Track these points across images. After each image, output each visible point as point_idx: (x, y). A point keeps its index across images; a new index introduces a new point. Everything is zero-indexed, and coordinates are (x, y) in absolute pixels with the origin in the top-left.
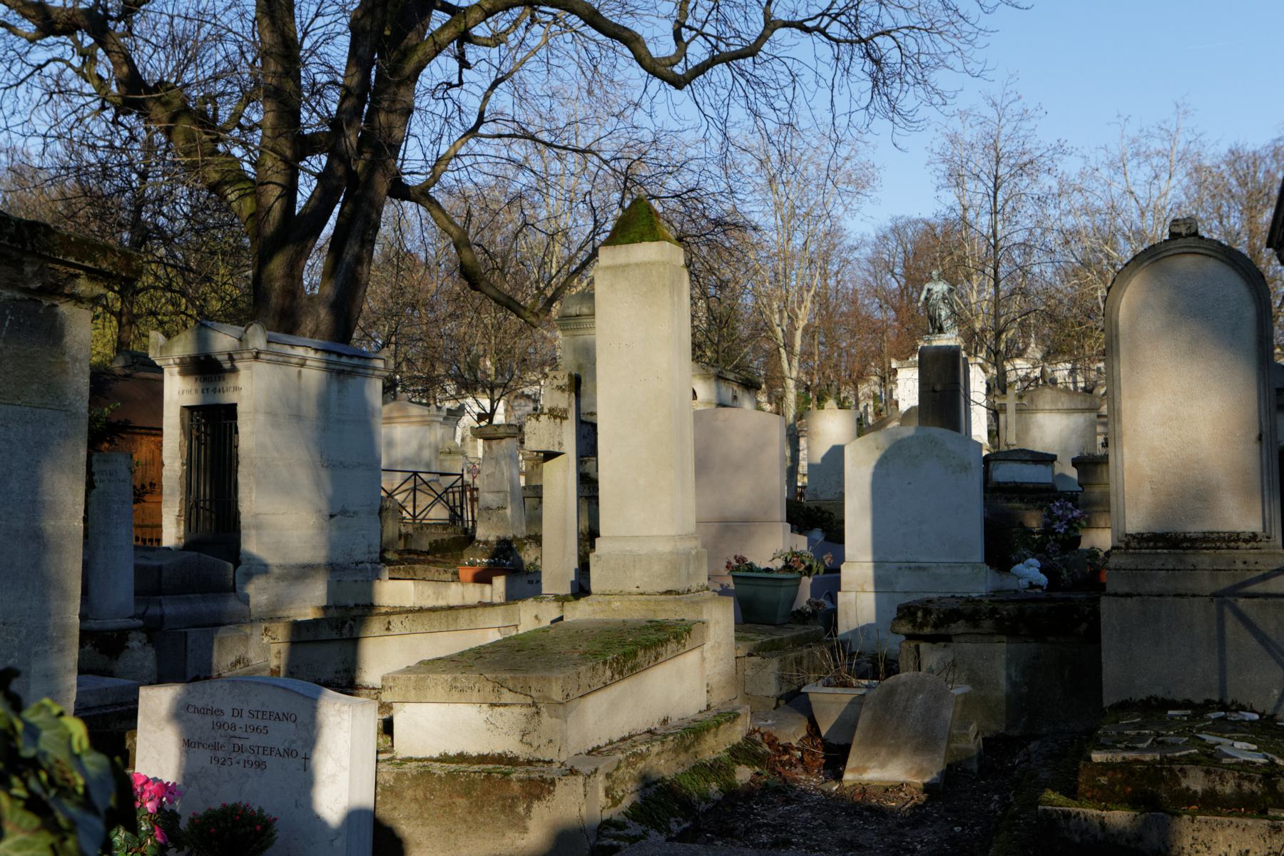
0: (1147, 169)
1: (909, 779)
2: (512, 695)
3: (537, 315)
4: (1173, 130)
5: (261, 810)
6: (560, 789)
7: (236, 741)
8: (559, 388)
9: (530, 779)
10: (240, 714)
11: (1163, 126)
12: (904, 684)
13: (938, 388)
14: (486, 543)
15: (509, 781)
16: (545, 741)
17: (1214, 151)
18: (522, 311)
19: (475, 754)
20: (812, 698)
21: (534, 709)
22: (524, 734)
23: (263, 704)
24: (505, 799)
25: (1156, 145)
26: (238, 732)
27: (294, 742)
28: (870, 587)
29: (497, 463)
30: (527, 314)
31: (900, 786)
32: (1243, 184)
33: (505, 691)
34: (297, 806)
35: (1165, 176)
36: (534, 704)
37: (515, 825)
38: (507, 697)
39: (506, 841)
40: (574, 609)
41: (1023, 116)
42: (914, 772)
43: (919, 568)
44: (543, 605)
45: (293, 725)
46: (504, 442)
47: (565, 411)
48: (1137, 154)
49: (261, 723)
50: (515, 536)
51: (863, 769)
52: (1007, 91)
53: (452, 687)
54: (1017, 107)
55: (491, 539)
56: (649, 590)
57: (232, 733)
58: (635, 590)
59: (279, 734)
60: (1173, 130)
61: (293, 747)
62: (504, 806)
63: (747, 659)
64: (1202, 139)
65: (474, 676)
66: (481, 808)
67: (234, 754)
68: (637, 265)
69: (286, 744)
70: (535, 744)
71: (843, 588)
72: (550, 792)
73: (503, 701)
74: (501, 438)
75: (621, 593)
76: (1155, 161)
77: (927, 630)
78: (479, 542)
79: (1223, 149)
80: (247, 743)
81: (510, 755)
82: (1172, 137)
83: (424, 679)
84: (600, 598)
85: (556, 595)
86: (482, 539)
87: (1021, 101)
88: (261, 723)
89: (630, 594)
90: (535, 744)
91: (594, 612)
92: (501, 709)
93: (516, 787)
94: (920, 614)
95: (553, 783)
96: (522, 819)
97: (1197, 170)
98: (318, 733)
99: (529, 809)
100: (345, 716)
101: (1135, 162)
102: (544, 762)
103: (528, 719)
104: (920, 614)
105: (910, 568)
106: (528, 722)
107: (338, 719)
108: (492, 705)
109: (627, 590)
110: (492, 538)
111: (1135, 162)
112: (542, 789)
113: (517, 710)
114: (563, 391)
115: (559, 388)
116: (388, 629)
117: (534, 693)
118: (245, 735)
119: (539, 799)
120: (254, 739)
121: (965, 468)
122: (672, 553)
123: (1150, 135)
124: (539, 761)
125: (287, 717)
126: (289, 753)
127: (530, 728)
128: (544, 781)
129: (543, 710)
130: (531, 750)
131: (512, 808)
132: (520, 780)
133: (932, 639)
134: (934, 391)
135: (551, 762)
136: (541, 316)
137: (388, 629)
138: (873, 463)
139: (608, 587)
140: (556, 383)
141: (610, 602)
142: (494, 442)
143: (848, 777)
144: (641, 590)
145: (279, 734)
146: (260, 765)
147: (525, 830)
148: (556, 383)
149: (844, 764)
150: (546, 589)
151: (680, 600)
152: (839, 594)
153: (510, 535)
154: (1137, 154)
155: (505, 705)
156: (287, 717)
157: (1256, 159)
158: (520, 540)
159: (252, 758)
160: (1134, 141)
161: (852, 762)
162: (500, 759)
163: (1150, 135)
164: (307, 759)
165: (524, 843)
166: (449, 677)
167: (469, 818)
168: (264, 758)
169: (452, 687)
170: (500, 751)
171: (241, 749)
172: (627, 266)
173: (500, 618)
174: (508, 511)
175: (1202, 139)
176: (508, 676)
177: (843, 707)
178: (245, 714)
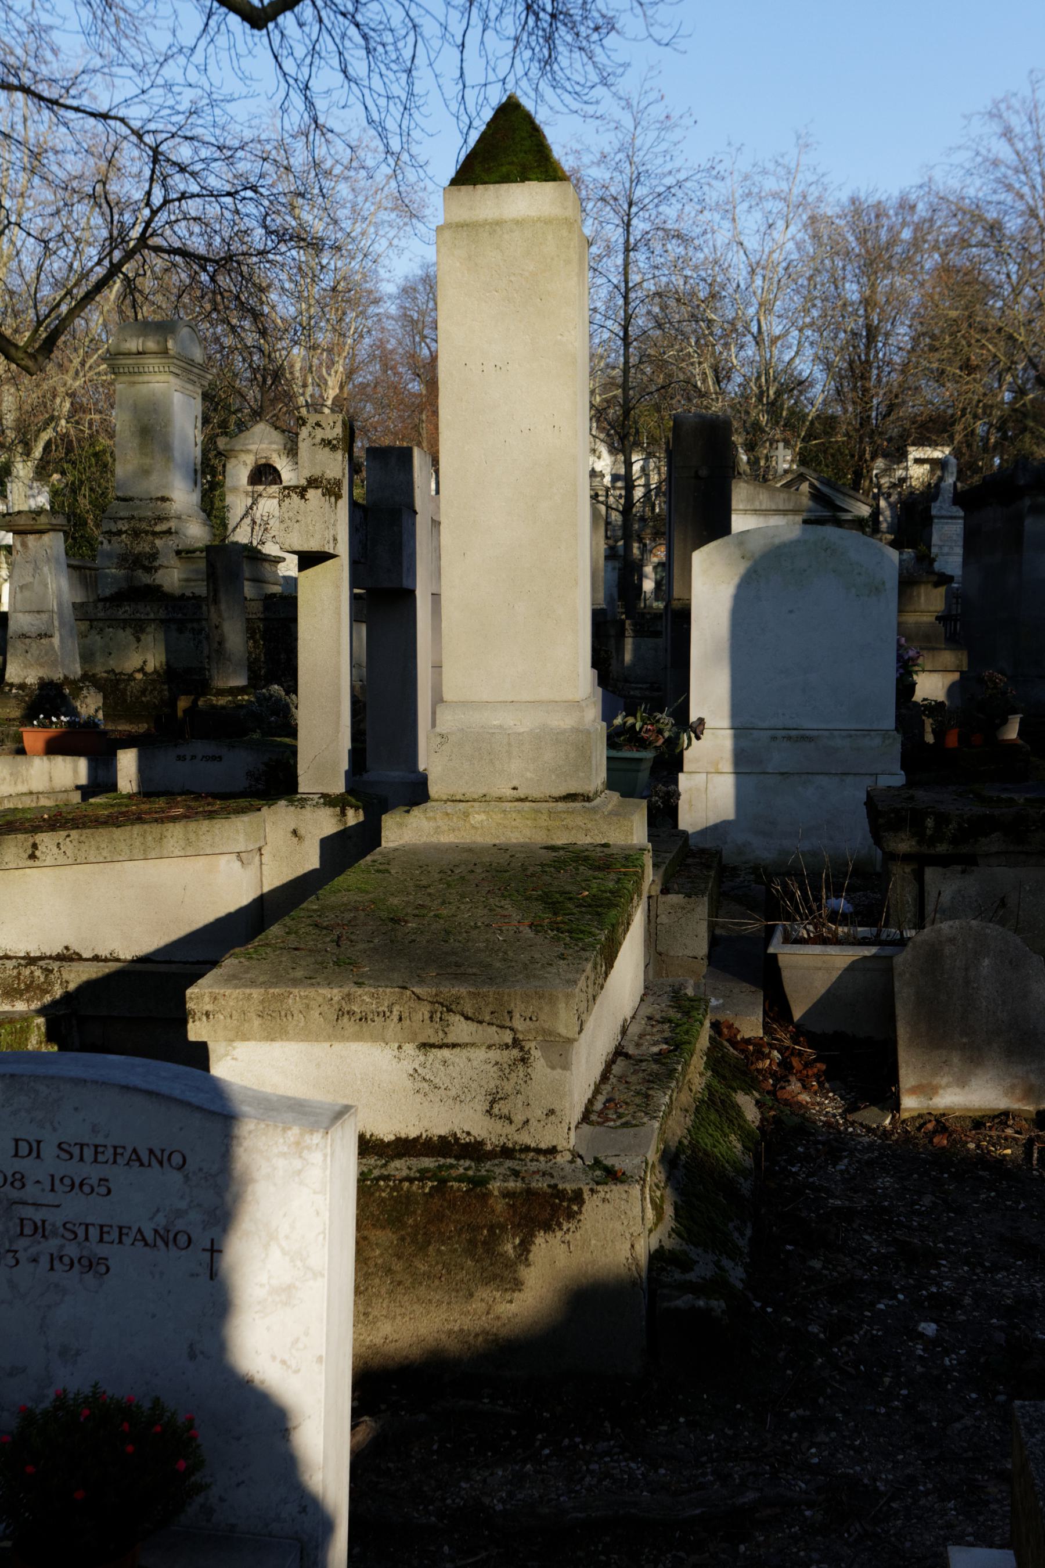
0: (757, 215)
1: (1016, 1106)
2: (472, 1026)
3: (33, 357)
4: (793, 165)
5: (156, 1402)
6: (593, 1210)
7: (28, 1212)
8: (326, 443)
9: (529, 1192)
10: (35, 1150)
11: (780, 160)
12: (952, 940)
13: (704, 472)
14: (22, 686)
15: (486, 1196)
16: (539, 1113)
17: (833, 203)
18: (13, 351)
19: (389, 1138)
20: (782, 961)
21: (515, 1053)
22: (494, 1099)
23: (95, 1130)
24: (475, 1229)
25: (770, 184)
26: (31, 1192)
27: (180, 1213)
28: (727, 766)
29: (36, 568)
30: (20, 355)
31: (1003, 1117)
32: (862, 241)
33: (456, 1019)
34: (192, 1356)
35: (780, 224)
36: (516, 1043)
37: (495, 1277)
38: (461, 1029)
39: (477, 1305)
40: (400, 825)
41: (667, 123)
42: (1018, 1092)
43: (803, 738)
44: (308, 813)
45: (178, 1177)
46: (46, 538)
47: (338, 483)
48: (749, 194)
49: (92, 1172)
50: (66, 678)
51: (926, 1090)
52: (647, 87)
53: (341, 1013)
54: (657, 112)
55: (30, 681)
56: (536, 794)
57: (15, 1194)
58: (509, 793)
59: (139, 1198)
60: (793, 165)
61: (180, 1224)
62: (473, 1242)
63: (662, 899)
64: (826, 180)
65: (389, 994)
66: (423, 1248)
67: (21, 1243)
68: (518, 222)
69: (161, 1220)
70: (519, 1118)
71: (685, 769)
72: (571, 1216)
73: (451, 1039)
74: (42, 532)
75: (484, 799)
76: (770, 205)
77: (942, 848)
78: (12, 685)
79: (844, 197)
80: (56, 1218)
81: (465, 1139)
82: (790, 174)
83: (281, 998)
84: (450, 807)
85: (324, 796)
86: (16, 681)
87: (663, 104)
88: (92, 1172)
89: (500, 799)
90: (519, 1118)
91: (437, 830)
92: (446, 1053)
93: (500, 1206)
94: (930, 822)
95: (578, 1197)
96: (511, 1265)
97: (813, 219)
98: (238, 1198)
99: (525, 1247)
100: (316, 1157)
101: (745, 205)
102: (538, 1151)
103: (504, 1072)
104: (930, 822)
105: (789, 738)
106: (504, 1077)
107: (297, 1164)
108: (425, 1046)
109: (496, 792)
110: (31, 680)
111: (745, 205)
112: (555, 1209)
113: (480, 1055)
114: (334, 448)
115: (326, 443)
116: (32, 857)
117: (518, 1024)
118: (50, 1198)
119: (547, 1227)
120: (75, 1208)
121: (876, 589)
122: (576, 730)
123: (765, 172)
124: (527, 1149)
125: (159, 1158)
126: (167, 1237)
127: (508, 1087)
128: (561, 1194)
129: (536, 1053)
130: (510, 1129)
131: (490, 1245)
132: (506, 1194)
133: (943, 861)
134: (697, 477)
135: (553, 1151)
136: (40, 358)
137: (32, 857)
138: (736, 580)
139: (459, 789)
140: (319, 434)
141: (466, 815)
142: (31, 537)
143: (910, 1103)
144: (521, 793)
145: (139, 1198)
146: (92, 1265)
147: (517, 1285)
148: (319, 434)
149: (895, 1080)
150: (305, 785)
151: (595, 810)
152: (681, 776)
153: (57, 676)
154: (749, 194)
155: (454, 1046)
156: (159, 1158)
157: (880, 213)
158: (74, 682)
159: (72, 1250)
160: (746, 178)
161: (908, 1077)
162: (444, 1146)
163: (765, 172)
164: (215, 1251)
165: (513, 1308)
166: (336, 993)
167: (398, 1266)
168: (102, 1250)
169: (341, 1013)
170: (443, 1131)
171: (40, 1230)
172: (499, 223)
173: (241, 838)
174: (56, 641)
175: (826, 180)
176: (463, 990)
177: (835, 975)
178: (49, 1150)
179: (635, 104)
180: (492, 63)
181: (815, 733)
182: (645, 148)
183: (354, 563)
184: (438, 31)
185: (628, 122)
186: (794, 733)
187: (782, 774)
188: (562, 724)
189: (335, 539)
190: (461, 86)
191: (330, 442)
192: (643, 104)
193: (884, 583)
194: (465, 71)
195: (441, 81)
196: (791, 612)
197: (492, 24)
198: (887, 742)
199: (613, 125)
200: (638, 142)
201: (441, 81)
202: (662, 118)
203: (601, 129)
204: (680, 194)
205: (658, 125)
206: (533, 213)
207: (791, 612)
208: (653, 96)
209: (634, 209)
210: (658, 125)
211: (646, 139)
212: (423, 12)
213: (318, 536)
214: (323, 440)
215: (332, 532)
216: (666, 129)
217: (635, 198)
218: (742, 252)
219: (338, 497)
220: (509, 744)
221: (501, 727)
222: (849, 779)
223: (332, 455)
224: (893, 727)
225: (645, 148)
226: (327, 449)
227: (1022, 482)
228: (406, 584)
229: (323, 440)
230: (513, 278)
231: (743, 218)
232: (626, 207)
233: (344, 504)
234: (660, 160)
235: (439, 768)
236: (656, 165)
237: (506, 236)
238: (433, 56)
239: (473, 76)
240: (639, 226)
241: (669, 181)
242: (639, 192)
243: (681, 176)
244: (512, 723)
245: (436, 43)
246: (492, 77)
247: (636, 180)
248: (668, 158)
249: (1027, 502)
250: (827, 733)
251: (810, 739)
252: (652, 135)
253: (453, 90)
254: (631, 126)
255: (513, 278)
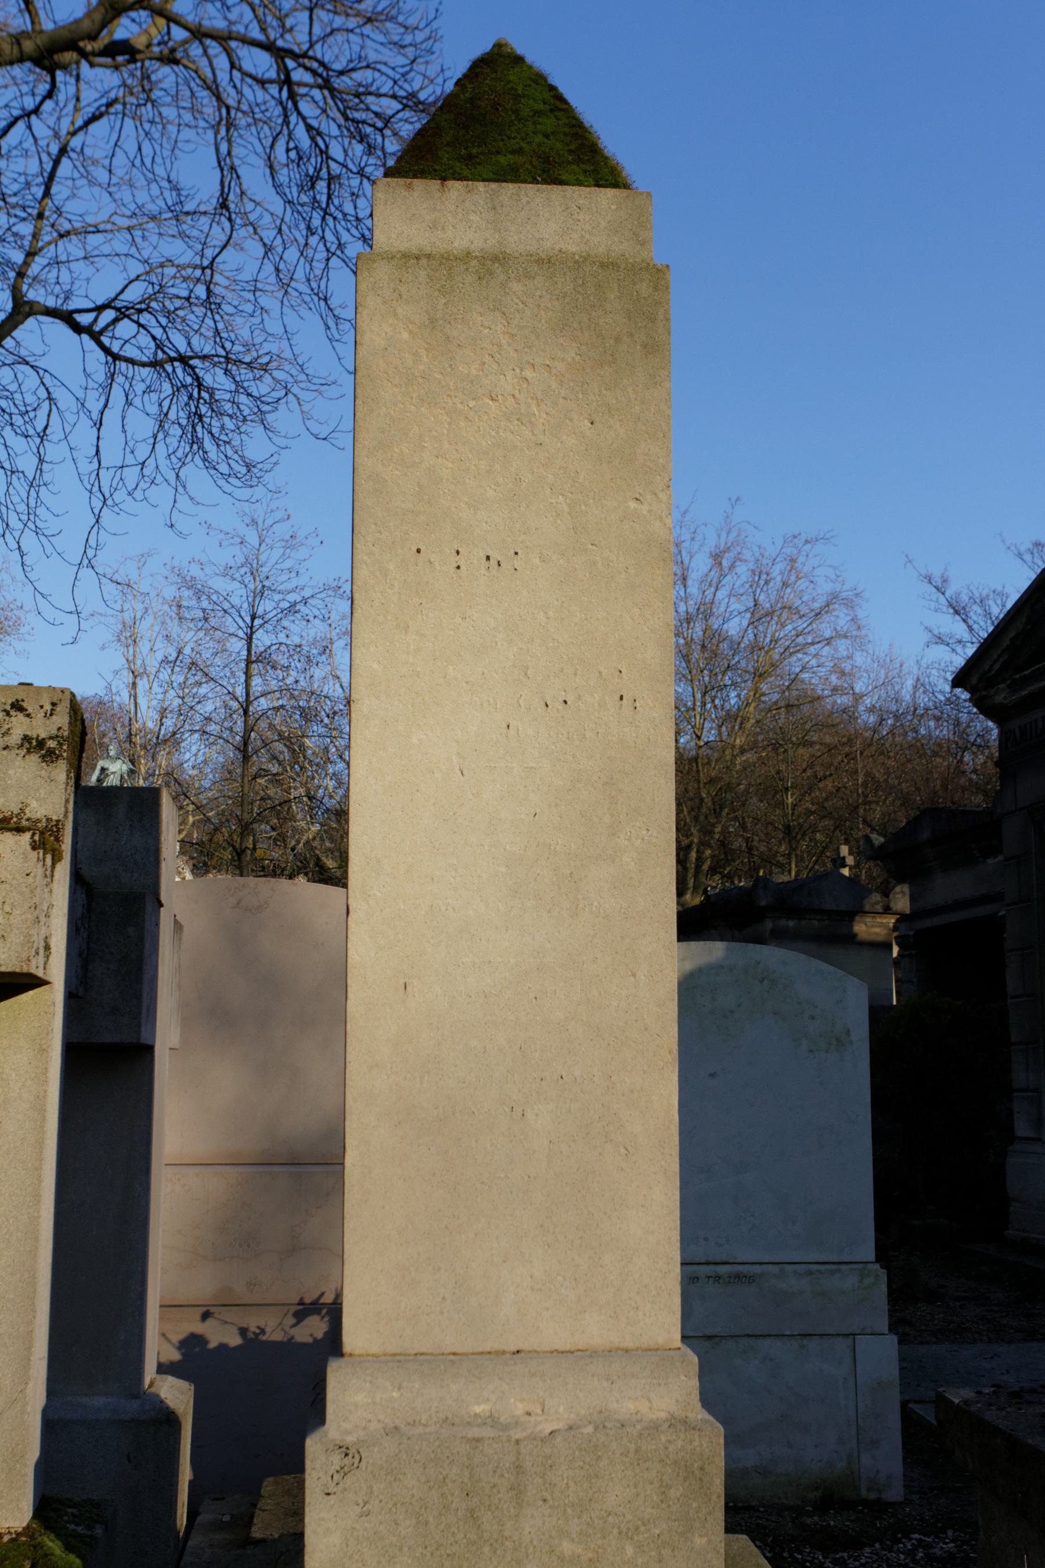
8: (33, 745)
41: (291, 542)
43: (738, 1277)
54: (282, 530)
105: (718, 1278)
114: (51, 757)
179: (260, 522)
180: (131, 444)
181: (757, 1269)
182: (269, 565)
183: (71, 996)
184: (74, 405)
185: (253, 538)
186: (722, 1270)
187: (709, 1338)
188: (644, 1407)
189: (47, 948)
190: (96, 465)
191: (41, 744)
192: (269, 522)
193: (848, 1032)
194: (101, 449)
195: (75, 454)
196: (712, 1075)
197: (137, 402)
198: (867, 1281)
199: (238, 540)
200: (263, 558)
201: (75, 454)
202: (287, 537)
203: (224, 543)
204: (304, 610)
205: (284, 544)
206: (572, 246)
207: (712, 1075)
208: (279, 515)
209: (257, 622)
210: (284, 544)
211: (270, 557)
212: (59, 384)
213: (16, 939)
214: (26, 738)
215: (43, 932)
216: (292, 547)
217: (260, 611)
218: (338, 685)
219: (57, 858)
220: (519, 1469)
221: (491, 1420)
222: (813, 1344)
223: (45, 770)
224: (872, 1257)
225: (269, 565)
226: (34, 758)
227: (763, 903)
228: (144, 1039)
229: (26, 738)
230: (529, 374)
231: (339, 655)
232: (248, 619)
233: (63, 871)
234: (284, 577)
235: (336, 1539)
236: (281, 580)
237: (516, 287)
238: (68, 429)
239: (111, 455)
240: (263, 639)
241: (293, 597)
242: (265, 606)
243: (307, 593)
244: (520, 1409)
245: (71, 418)
246: (130, 460)
247: (260, 593)
248: (293, 574)
249: (769, 925)
250: (774, 1269)
251: (750, 1279)
252: (277, 553)
253: (87, 467)
254: (256, 542)
255: (529, 374)
